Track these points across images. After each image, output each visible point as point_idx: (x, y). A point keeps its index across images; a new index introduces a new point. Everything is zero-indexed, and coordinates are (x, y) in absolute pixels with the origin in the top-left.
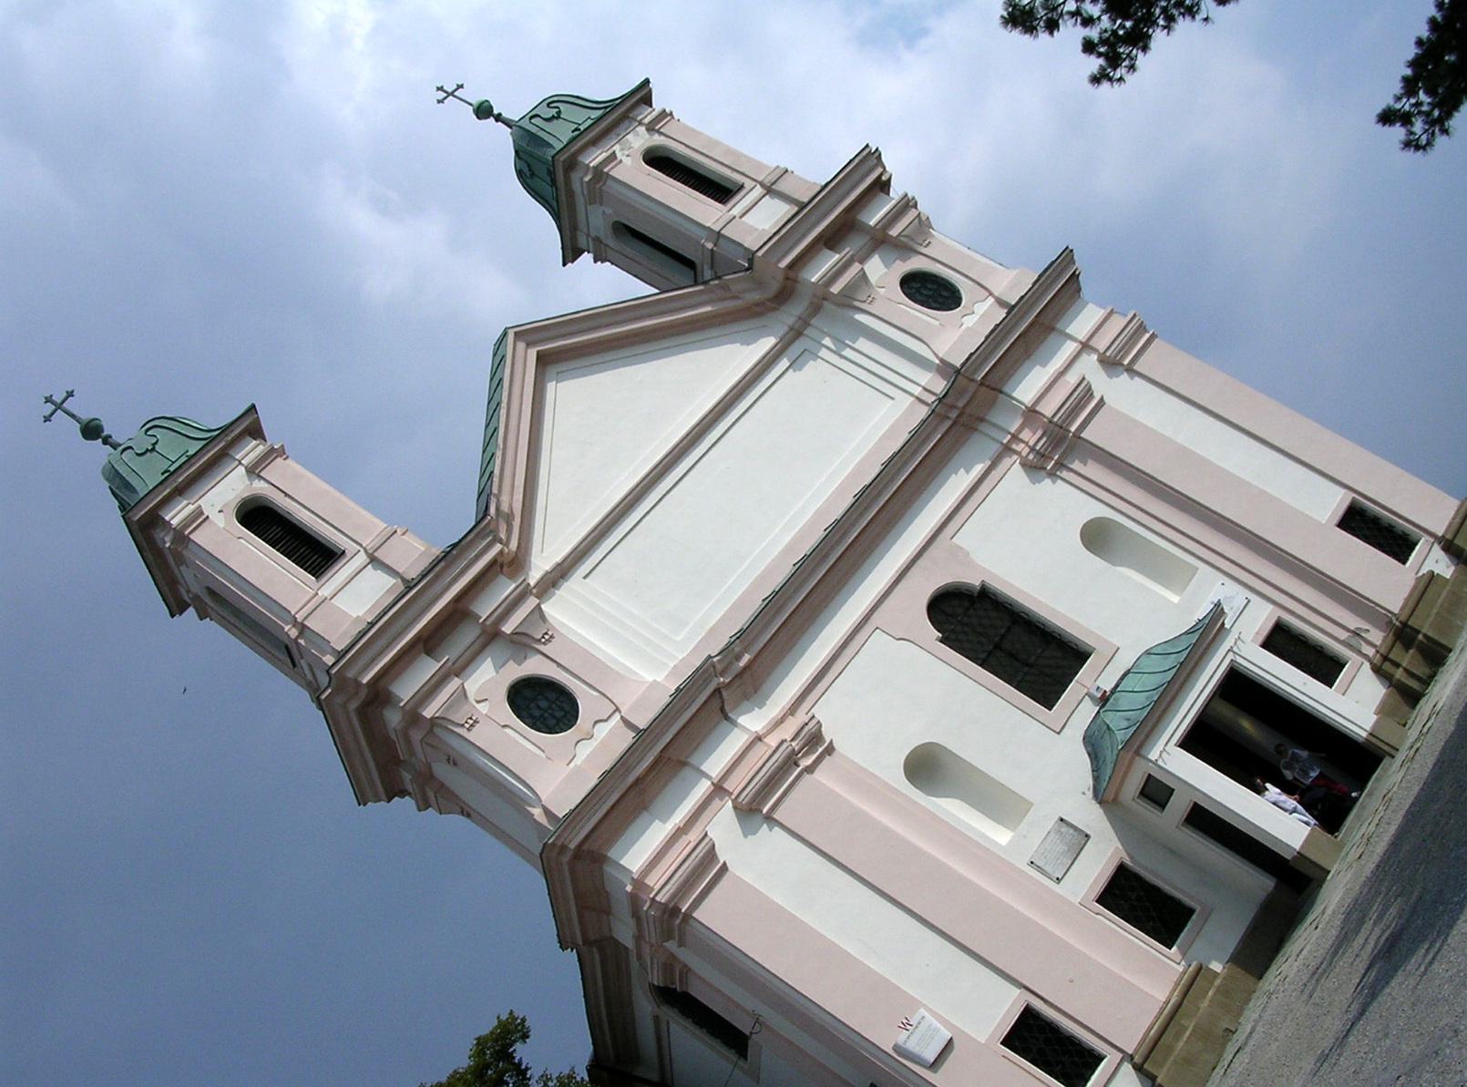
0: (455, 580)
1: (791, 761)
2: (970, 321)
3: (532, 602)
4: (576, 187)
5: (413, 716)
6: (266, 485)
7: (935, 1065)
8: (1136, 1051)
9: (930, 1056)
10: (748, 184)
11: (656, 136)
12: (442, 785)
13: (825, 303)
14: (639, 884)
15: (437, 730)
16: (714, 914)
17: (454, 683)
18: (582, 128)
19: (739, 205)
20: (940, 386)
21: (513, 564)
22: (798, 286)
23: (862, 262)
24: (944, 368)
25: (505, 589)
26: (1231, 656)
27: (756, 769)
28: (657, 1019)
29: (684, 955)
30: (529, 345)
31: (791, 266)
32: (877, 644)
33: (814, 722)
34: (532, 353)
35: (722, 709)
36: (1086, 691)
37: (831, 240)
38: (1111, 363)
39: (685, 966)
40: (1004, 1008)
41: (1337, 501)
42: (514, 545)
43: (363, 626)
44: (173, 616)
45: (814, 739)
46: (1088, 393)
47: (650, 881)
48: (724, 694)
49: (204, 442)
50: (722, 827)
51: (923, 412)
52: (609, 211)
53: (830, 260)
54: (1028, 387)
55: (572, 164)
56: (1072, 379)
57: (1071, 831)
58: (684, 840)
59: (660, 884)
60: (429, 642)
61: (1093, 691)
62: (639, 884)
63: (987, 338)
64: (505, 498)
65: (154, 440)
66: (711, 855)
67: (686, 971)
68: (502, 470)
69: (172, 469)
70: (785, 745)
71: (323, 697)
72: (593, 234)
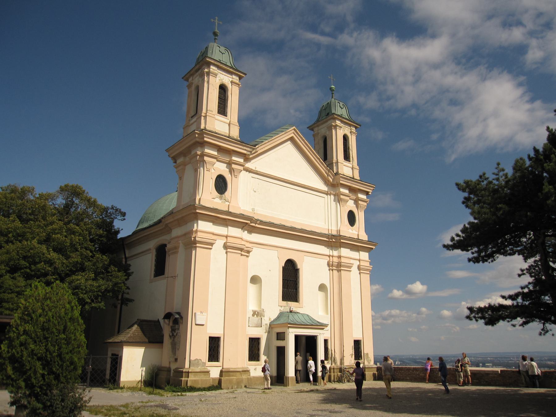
0: (356, 185)
1: (241, 250)
2: (350, 231)
3: (241, 168)
4: (329, 122)
5: (203, 155)
6: (231, 88)
7: (196, 325)
8: (225, 369)
9: (197, 323)
10: (351, 162)
11: (350, 134)
12: (185, 169)
13: (337, 196)
14: (196, 231)
15: (202, 163)
16: (199, 254)
17: (215, 160)
18: (343, 116)
19: (346, 163)
20: (334, 233)
21: (247, 159)
22: (337, 188)
23: (350, 199)
24: (339, 231)
25: (241, 160)
26: (319, 334)
27: (235, 243)
28: (150, 249)
29: (181, 250)
30: (294, 133)
31: (341, 184)
32: (274, 253)
33: (252, 249)
34: (293, 135)
35: (243, 227)
36: (290, 306)
37: (351, 189)
38: (359, 268)
39: (178, 252)
40: (216, 332)
41: (358, 337)
42: (251, 156)
43: (214, 130)
44: (183, 78)
45: (248, 252)
46: (350, 267)
47: (199, 233)
48: (247, 226)
49: (231, 66)
50: (220, 243)
51: (327, 232)
52: (327, 133)
53: (346, 191)
54: (345, 252)
55: (335, 119)
56: (352, 261)
57: (260, 322)
58: (211, 235)
59: (200, 237)
60: (220, 149)
61: (292, 308)
62: (196, 231)
63: (349, 237)
64: (260, 148)
65: (225, 53)
66: (212, 244)
67: (176, 253)
68: (265, 144)
69: (221, 62)
70: (244, 246)
71: (196, 131)
72: (319, 131)
